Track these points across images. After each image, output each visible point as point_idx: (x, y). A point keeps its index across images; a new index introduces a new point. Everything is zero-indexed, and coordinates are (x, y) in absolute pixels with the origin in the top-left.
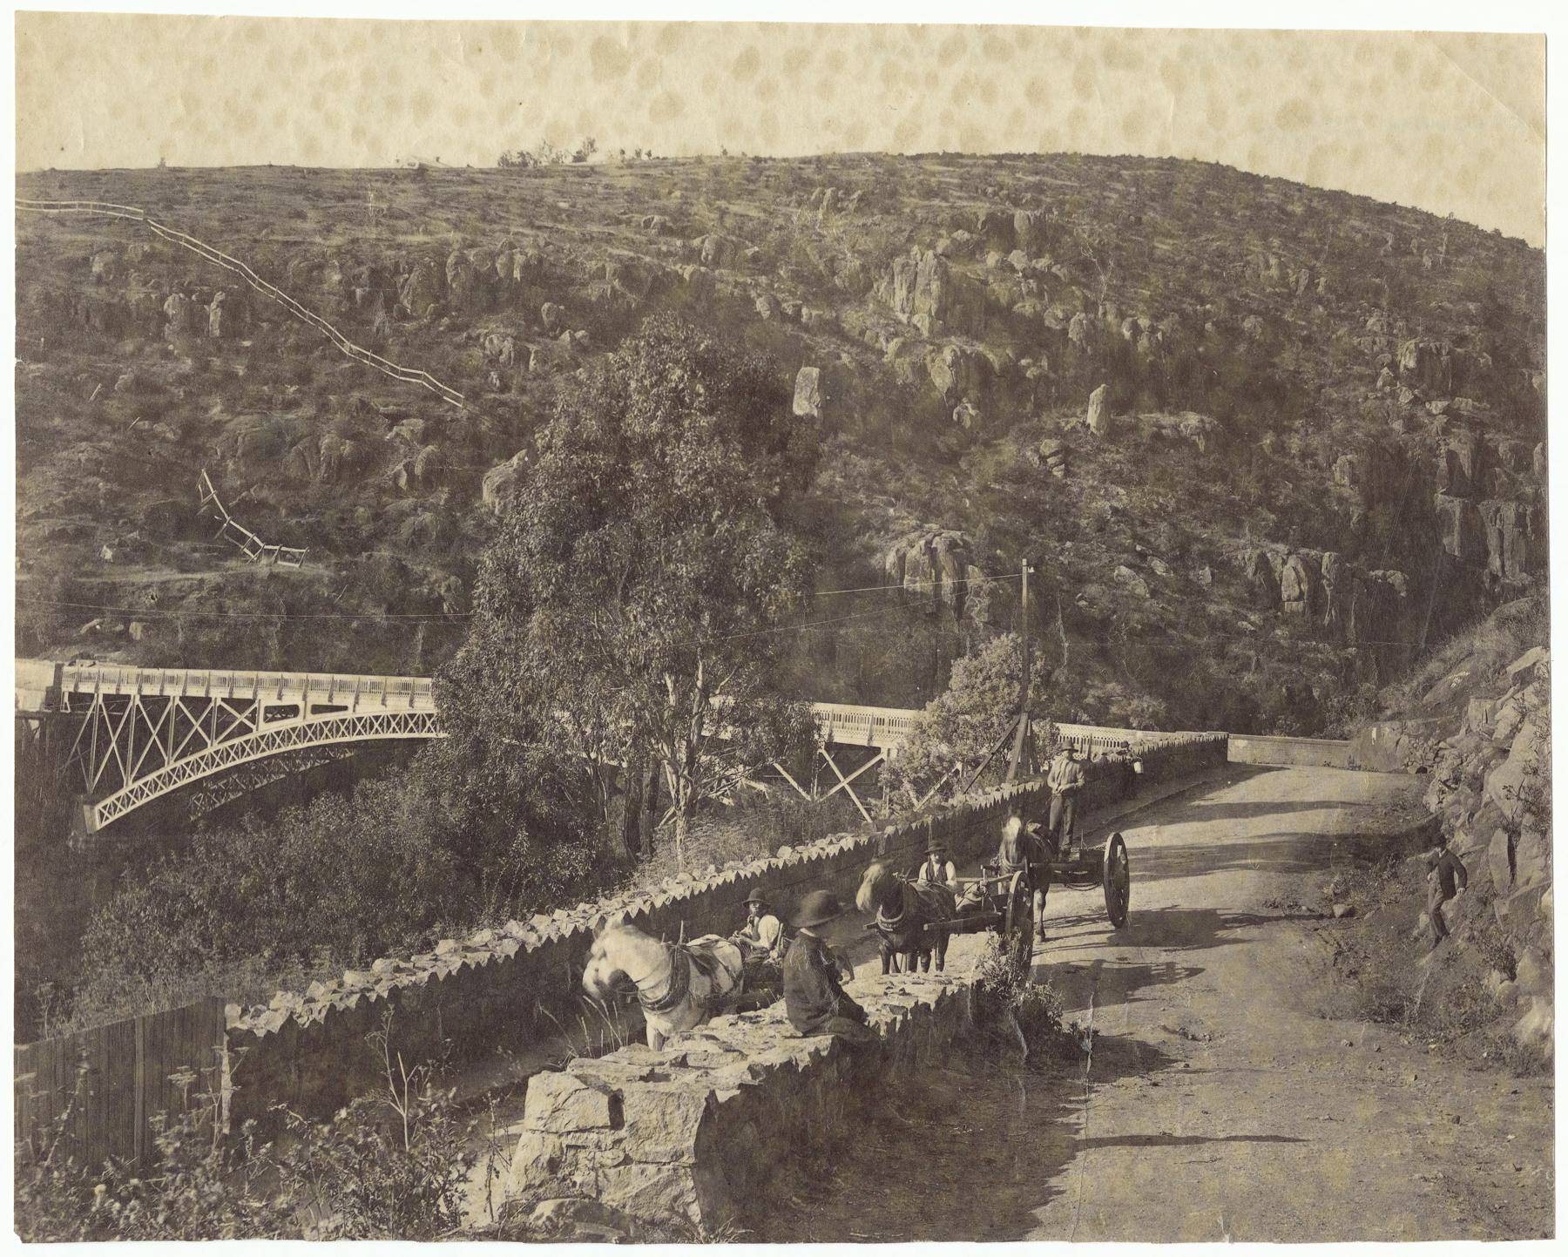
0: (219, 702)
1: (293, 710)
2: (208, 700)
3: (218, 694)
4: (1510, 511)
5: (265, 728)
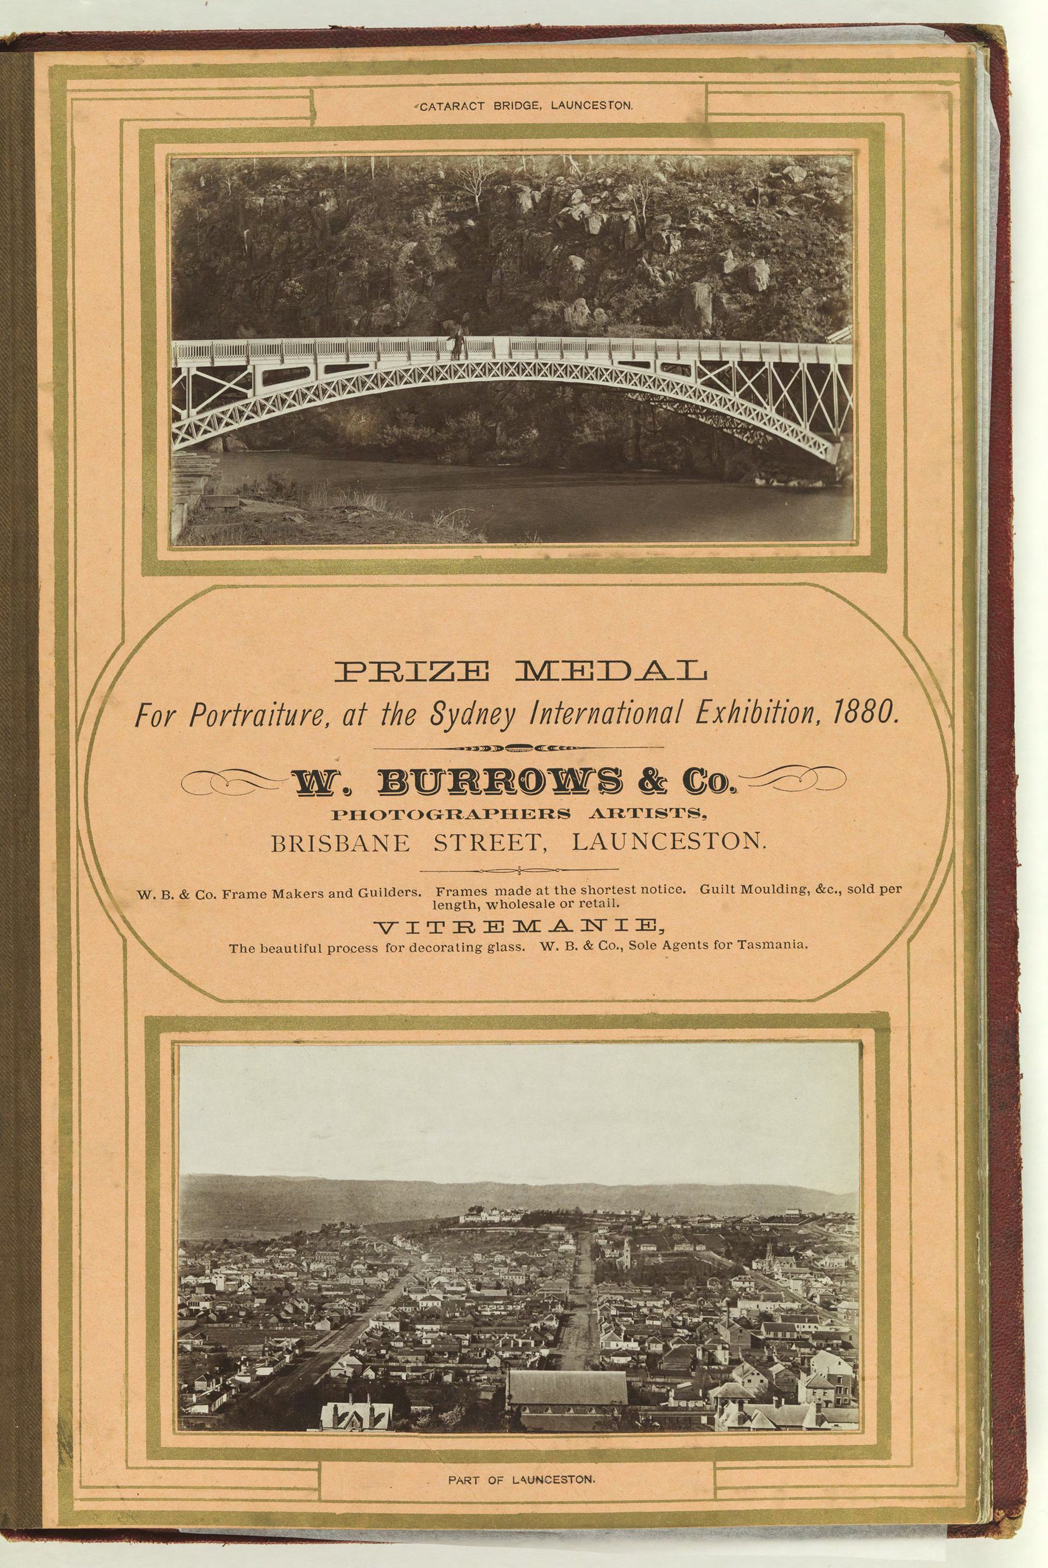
0: (194, 372)
1: (304, 372)
2: (762, 364)
3: (770, 360)
4: (647, 1259)
5: (262, 391)
